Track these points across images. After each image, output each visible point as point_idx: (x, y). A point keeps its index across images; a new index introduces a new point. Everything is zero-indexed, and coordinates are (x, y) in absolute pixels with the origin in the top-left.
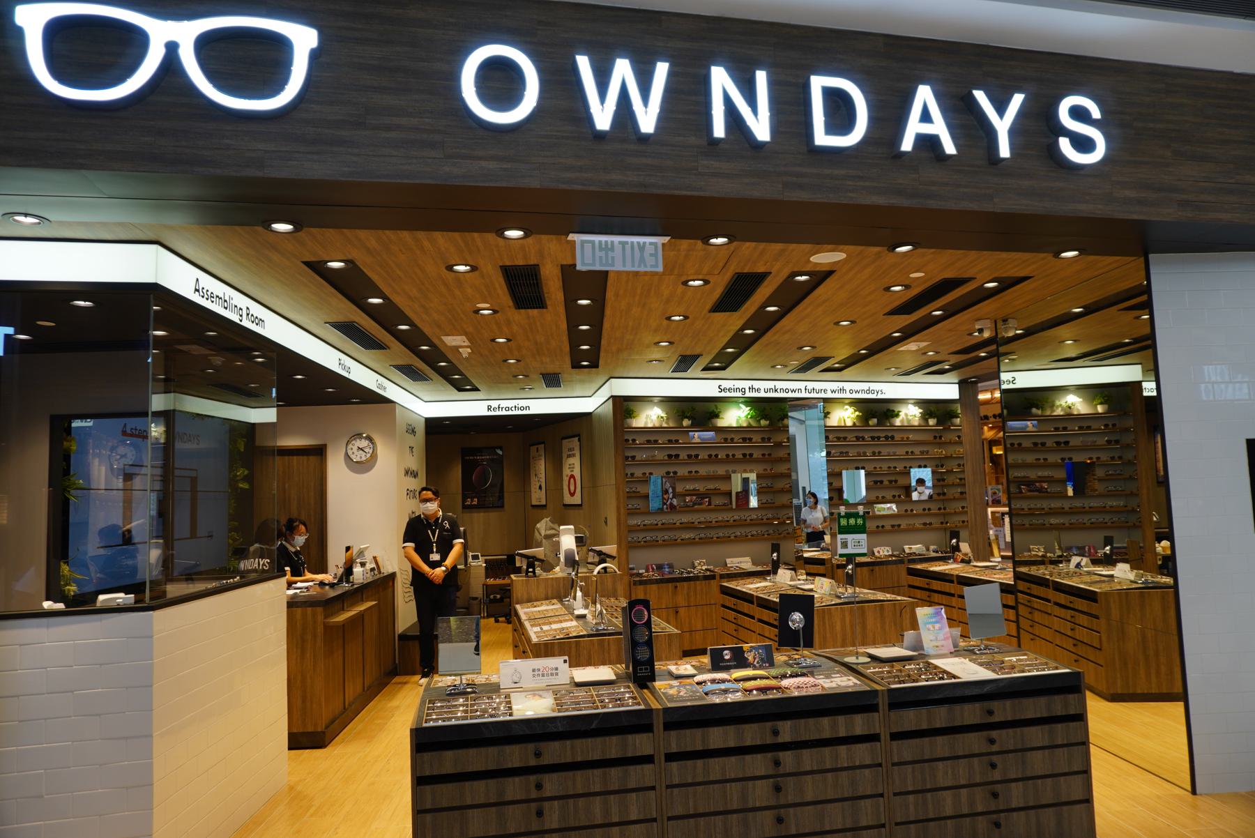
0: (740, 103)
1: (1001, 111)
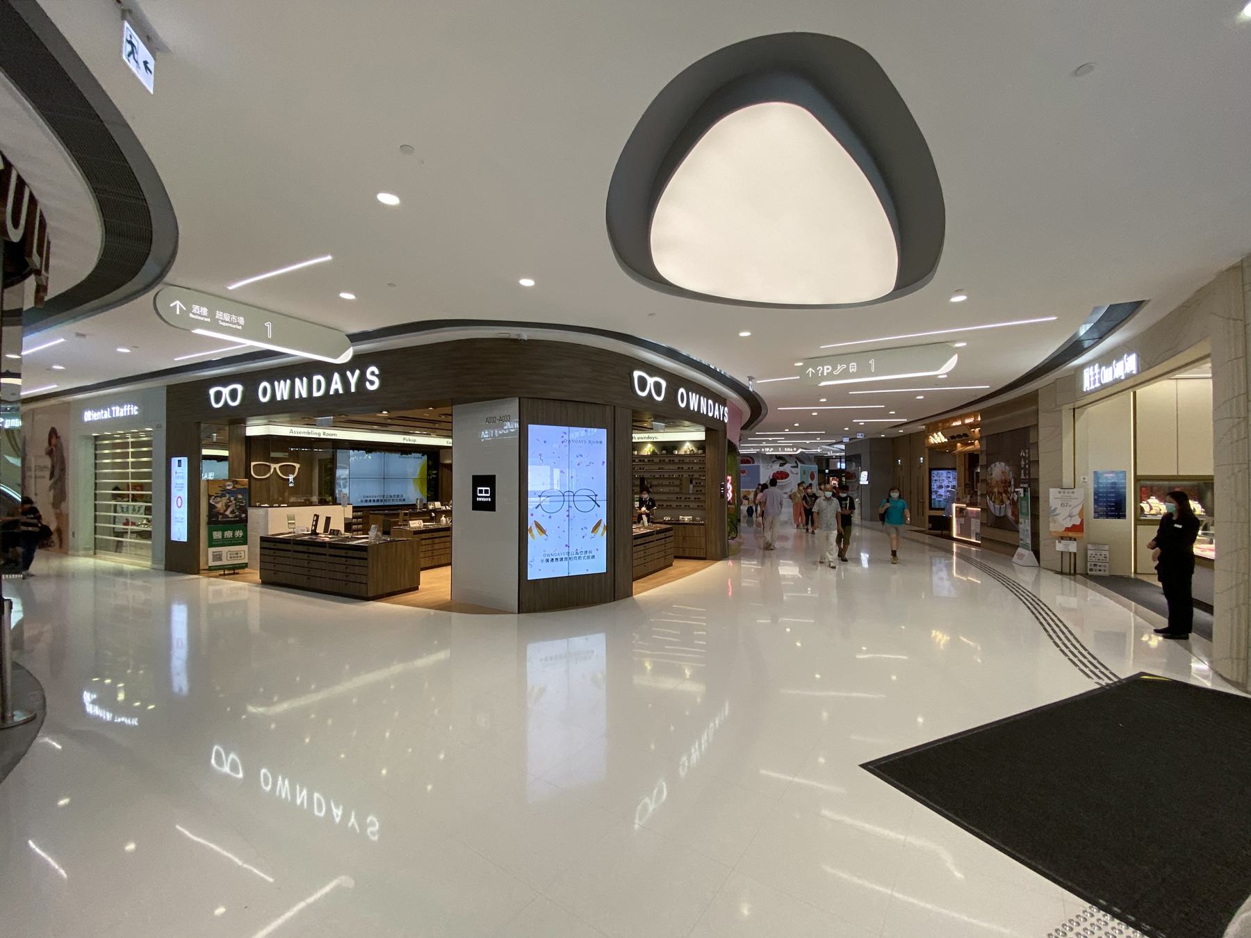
0: (301, 388)
1: (353, 374)
